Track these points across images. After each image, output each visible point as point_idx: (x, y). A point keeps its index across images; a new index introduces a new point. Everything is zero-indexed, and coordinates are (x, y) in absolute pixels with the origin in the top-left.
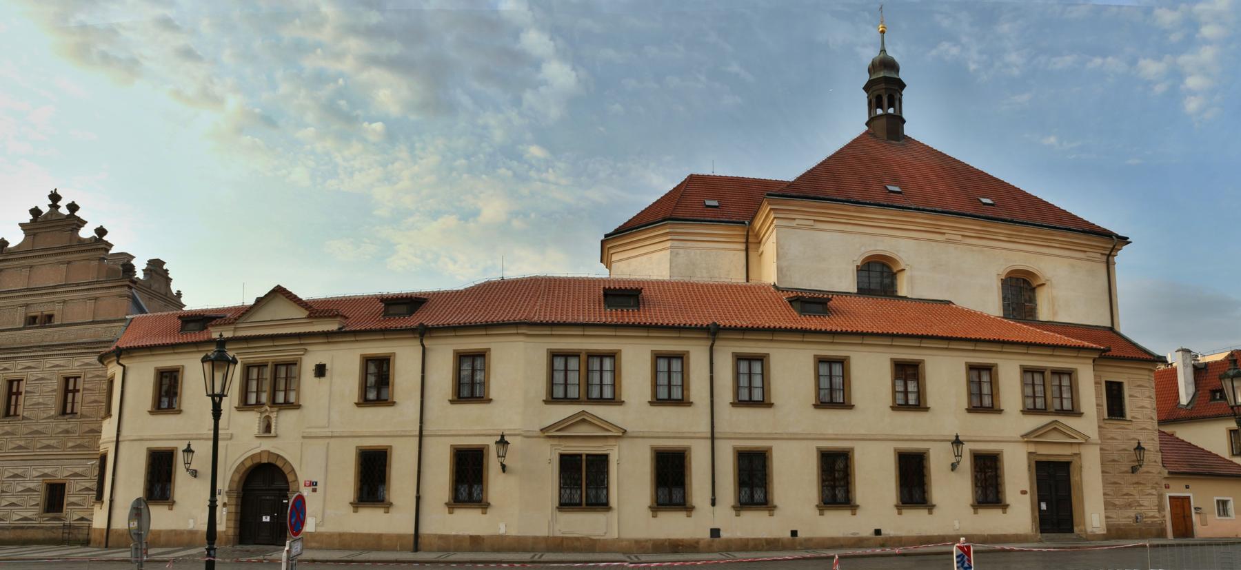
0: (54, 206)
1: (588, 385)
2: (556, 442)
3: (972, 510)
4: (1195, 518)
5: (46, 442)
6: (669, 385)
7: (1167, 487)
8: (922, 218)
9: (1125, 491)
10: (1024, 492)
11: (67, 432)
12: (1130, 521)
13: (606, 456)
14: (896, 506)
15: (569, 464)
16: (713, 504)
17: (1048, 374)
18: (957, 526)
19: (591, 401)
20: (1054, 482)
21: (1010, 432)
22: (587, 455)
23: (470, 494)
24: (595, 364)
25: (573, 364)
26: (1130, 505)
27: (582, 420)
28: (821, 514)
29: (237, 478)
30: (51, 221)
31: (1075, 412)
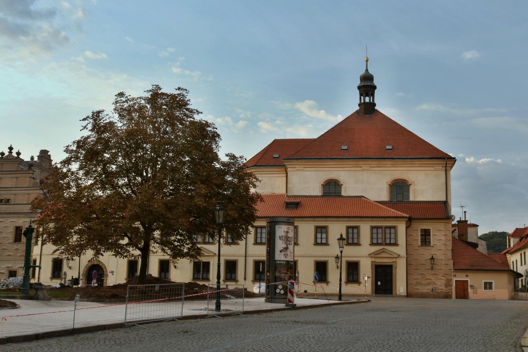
0: (10, 152)
1: (385, 238)
4: (470, 290)
5: (8, 253)
6: (353, 238)
7: (455, 276)
8: (350, 162)
9: (428, 277)
11: (17, 249)
12: (429, 291)
16: (245, 279)
17: (383, 228)
19: (387, 244)
20: (384, 277)
21: (364, 254)
22: (204, 262)
23: (231, 277)
24: (388, 231)
25: (380, 231)
26: (429, 284)
27: (383, 251)
29: (85, 270)
30: (9, 159)
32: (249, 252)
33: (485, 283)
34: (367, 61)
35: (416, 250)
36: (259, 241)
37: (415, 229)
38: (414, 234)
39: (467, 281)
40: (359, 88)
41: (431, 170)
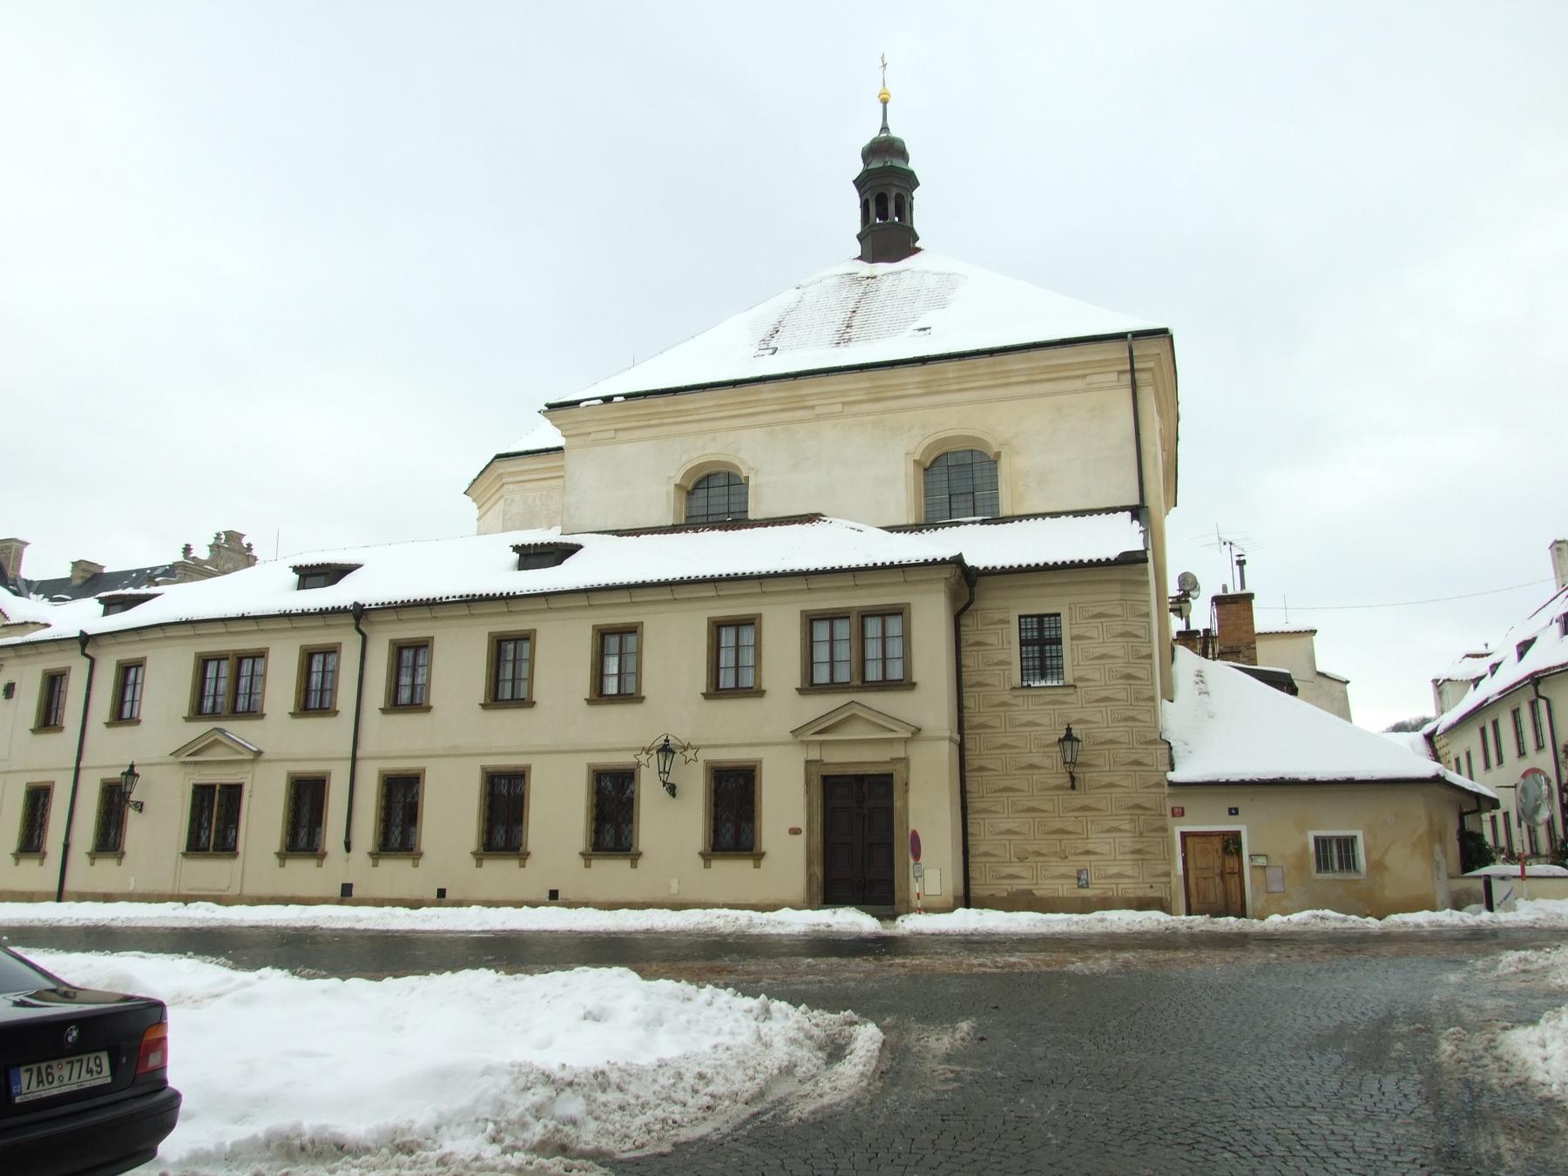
1: (863, 661)
2: (190, 769)
3: (276, 861)
7: (1179, 813)
10: (795, 831)
13: (891, 776)
14: (474, 854)
15: (202, 793)
16: (348, 848)
18: (674, 890)
19: (867, 686)
22: (224, 786)
25: (843, 629)
28: (479, 865)
31: (906, 684)
32: (367, 746)
33: (1322, 843)
34: (885, 102)
35: (1004, 704)
36: (822, 676)
37: (997, 616)
38: (993, 640)
39: (1237, 835)
40: (860, 183)
41: (1076, 391)
